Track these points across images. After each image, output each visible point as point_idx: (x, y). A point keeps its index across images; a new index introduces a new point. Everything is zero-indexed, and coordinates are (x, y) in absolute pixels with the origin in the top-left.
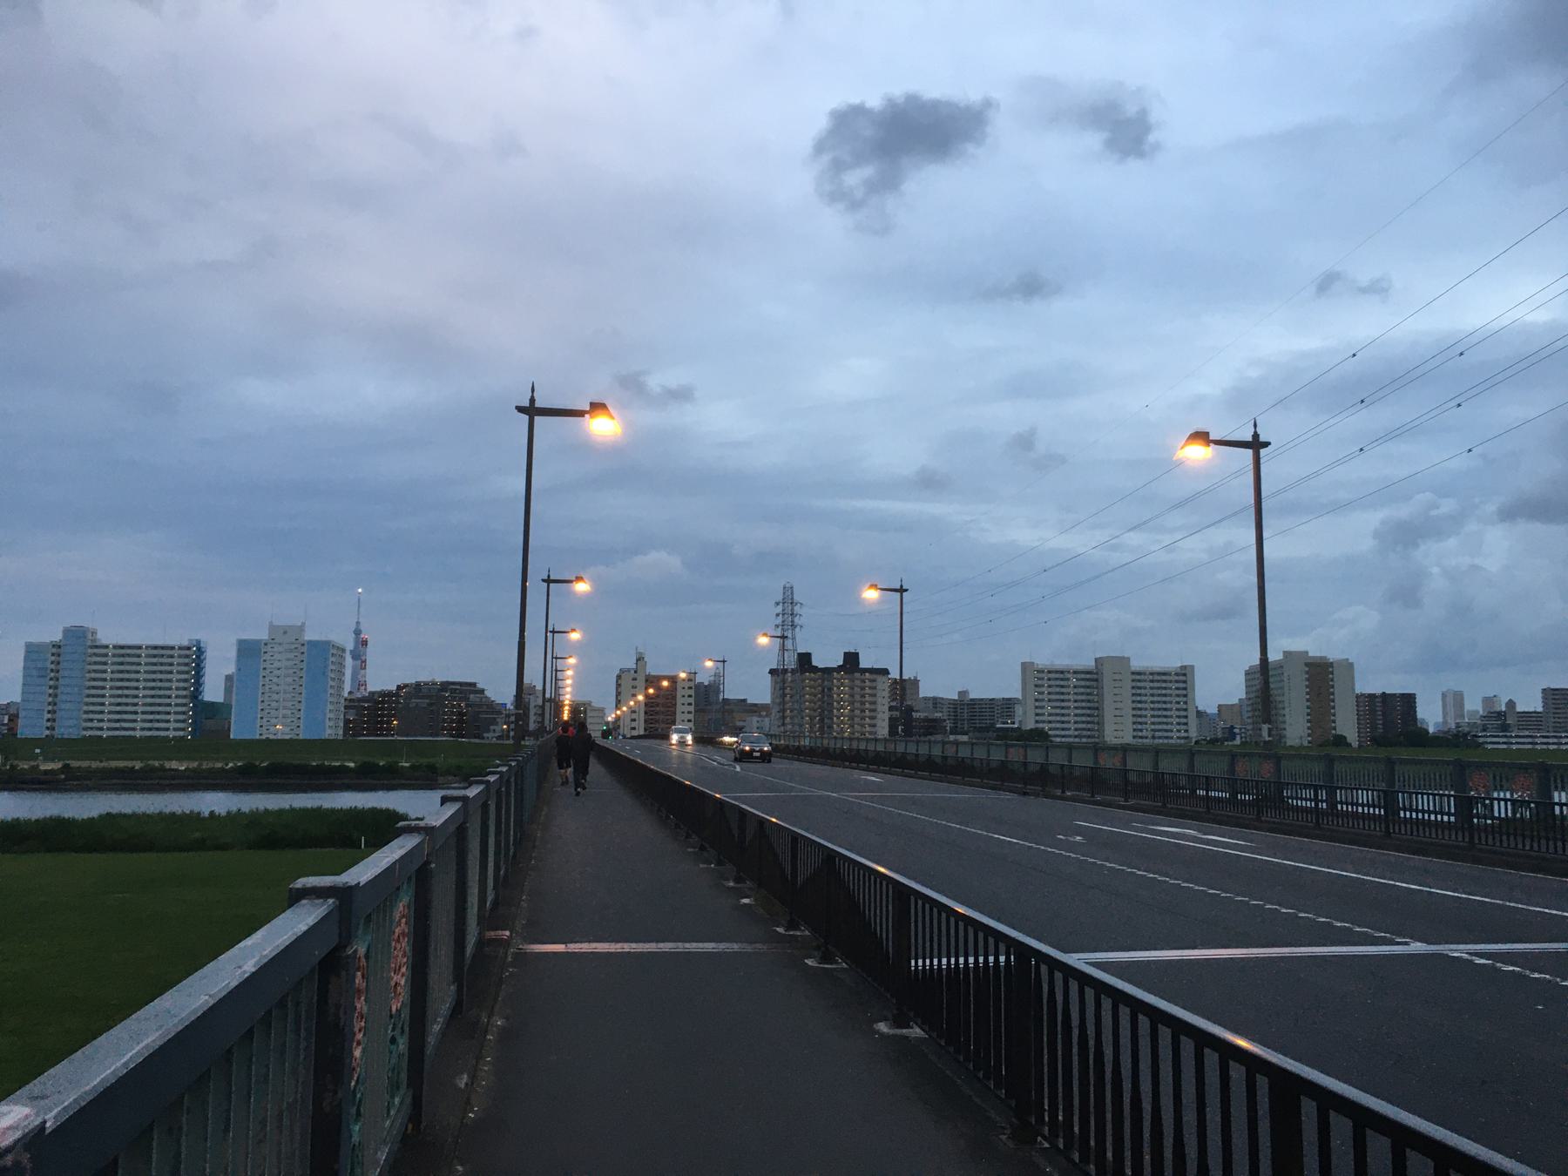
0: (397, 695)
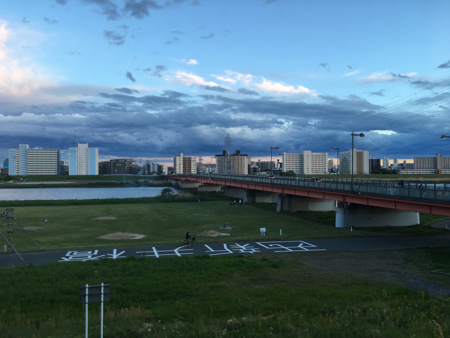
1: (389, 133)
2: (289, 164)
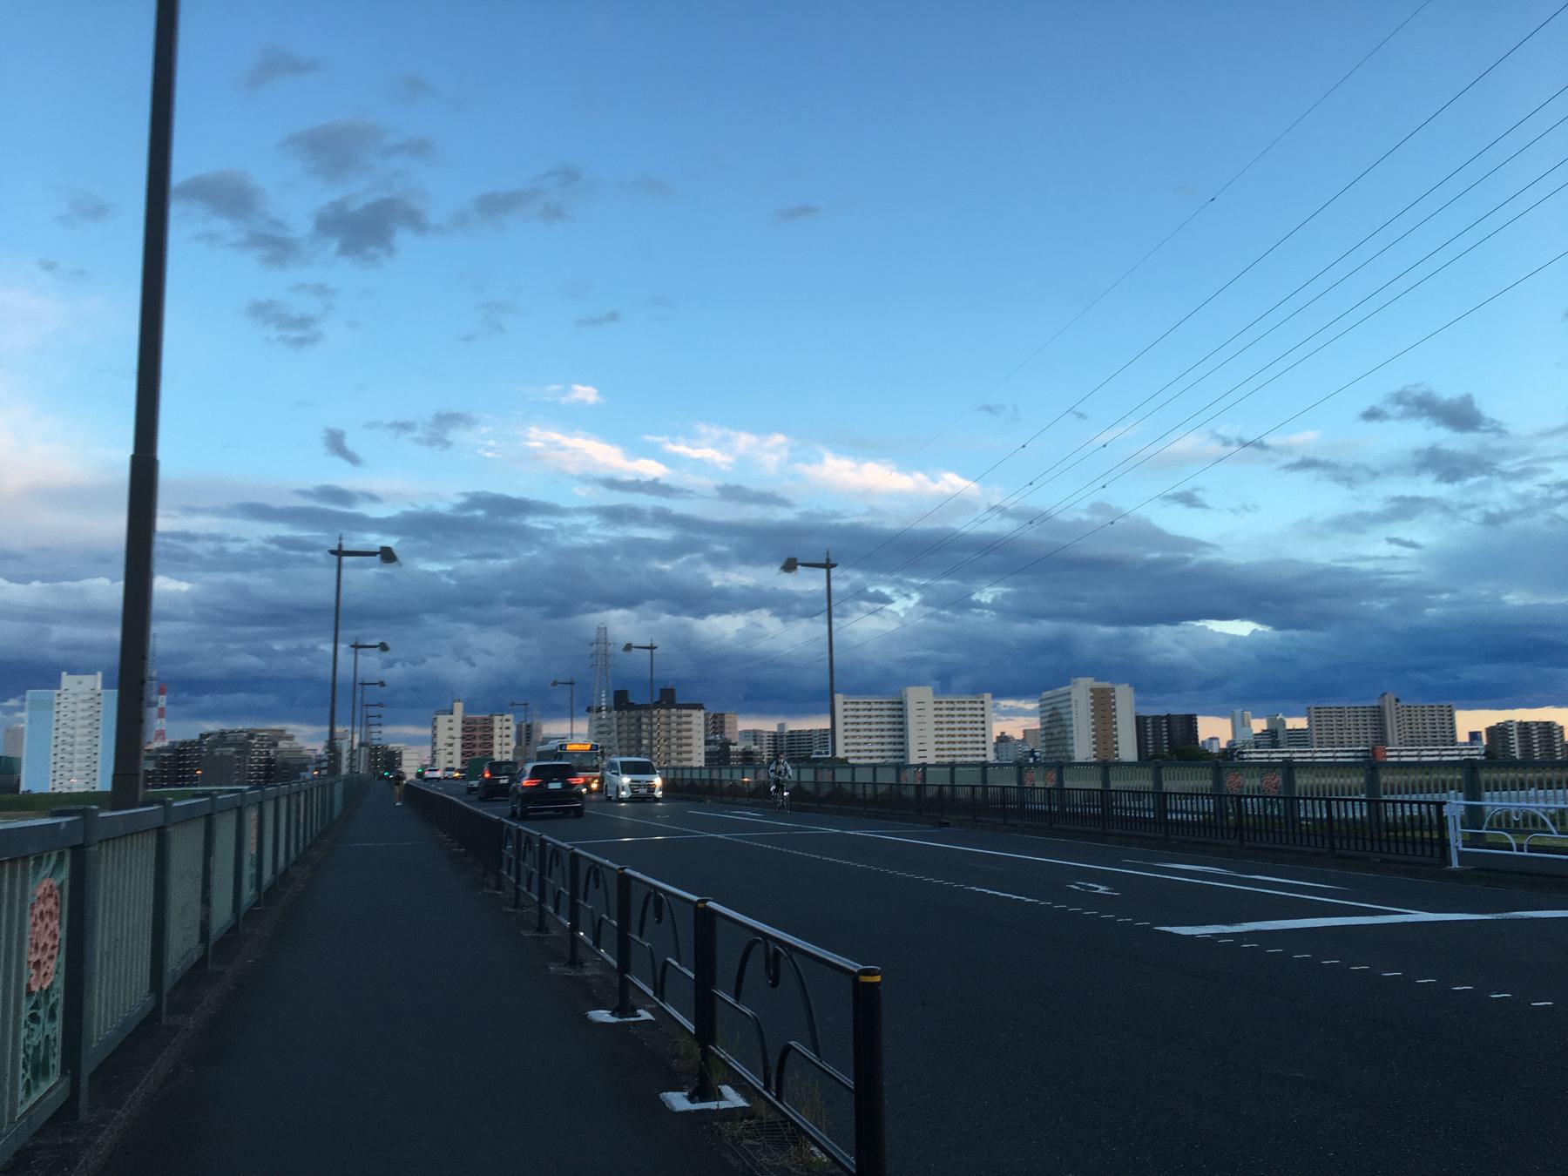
0: (199, 743)
1: (1241, 628)
2: (854, 734)
